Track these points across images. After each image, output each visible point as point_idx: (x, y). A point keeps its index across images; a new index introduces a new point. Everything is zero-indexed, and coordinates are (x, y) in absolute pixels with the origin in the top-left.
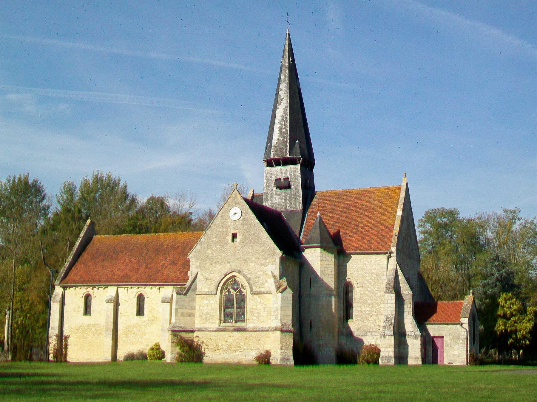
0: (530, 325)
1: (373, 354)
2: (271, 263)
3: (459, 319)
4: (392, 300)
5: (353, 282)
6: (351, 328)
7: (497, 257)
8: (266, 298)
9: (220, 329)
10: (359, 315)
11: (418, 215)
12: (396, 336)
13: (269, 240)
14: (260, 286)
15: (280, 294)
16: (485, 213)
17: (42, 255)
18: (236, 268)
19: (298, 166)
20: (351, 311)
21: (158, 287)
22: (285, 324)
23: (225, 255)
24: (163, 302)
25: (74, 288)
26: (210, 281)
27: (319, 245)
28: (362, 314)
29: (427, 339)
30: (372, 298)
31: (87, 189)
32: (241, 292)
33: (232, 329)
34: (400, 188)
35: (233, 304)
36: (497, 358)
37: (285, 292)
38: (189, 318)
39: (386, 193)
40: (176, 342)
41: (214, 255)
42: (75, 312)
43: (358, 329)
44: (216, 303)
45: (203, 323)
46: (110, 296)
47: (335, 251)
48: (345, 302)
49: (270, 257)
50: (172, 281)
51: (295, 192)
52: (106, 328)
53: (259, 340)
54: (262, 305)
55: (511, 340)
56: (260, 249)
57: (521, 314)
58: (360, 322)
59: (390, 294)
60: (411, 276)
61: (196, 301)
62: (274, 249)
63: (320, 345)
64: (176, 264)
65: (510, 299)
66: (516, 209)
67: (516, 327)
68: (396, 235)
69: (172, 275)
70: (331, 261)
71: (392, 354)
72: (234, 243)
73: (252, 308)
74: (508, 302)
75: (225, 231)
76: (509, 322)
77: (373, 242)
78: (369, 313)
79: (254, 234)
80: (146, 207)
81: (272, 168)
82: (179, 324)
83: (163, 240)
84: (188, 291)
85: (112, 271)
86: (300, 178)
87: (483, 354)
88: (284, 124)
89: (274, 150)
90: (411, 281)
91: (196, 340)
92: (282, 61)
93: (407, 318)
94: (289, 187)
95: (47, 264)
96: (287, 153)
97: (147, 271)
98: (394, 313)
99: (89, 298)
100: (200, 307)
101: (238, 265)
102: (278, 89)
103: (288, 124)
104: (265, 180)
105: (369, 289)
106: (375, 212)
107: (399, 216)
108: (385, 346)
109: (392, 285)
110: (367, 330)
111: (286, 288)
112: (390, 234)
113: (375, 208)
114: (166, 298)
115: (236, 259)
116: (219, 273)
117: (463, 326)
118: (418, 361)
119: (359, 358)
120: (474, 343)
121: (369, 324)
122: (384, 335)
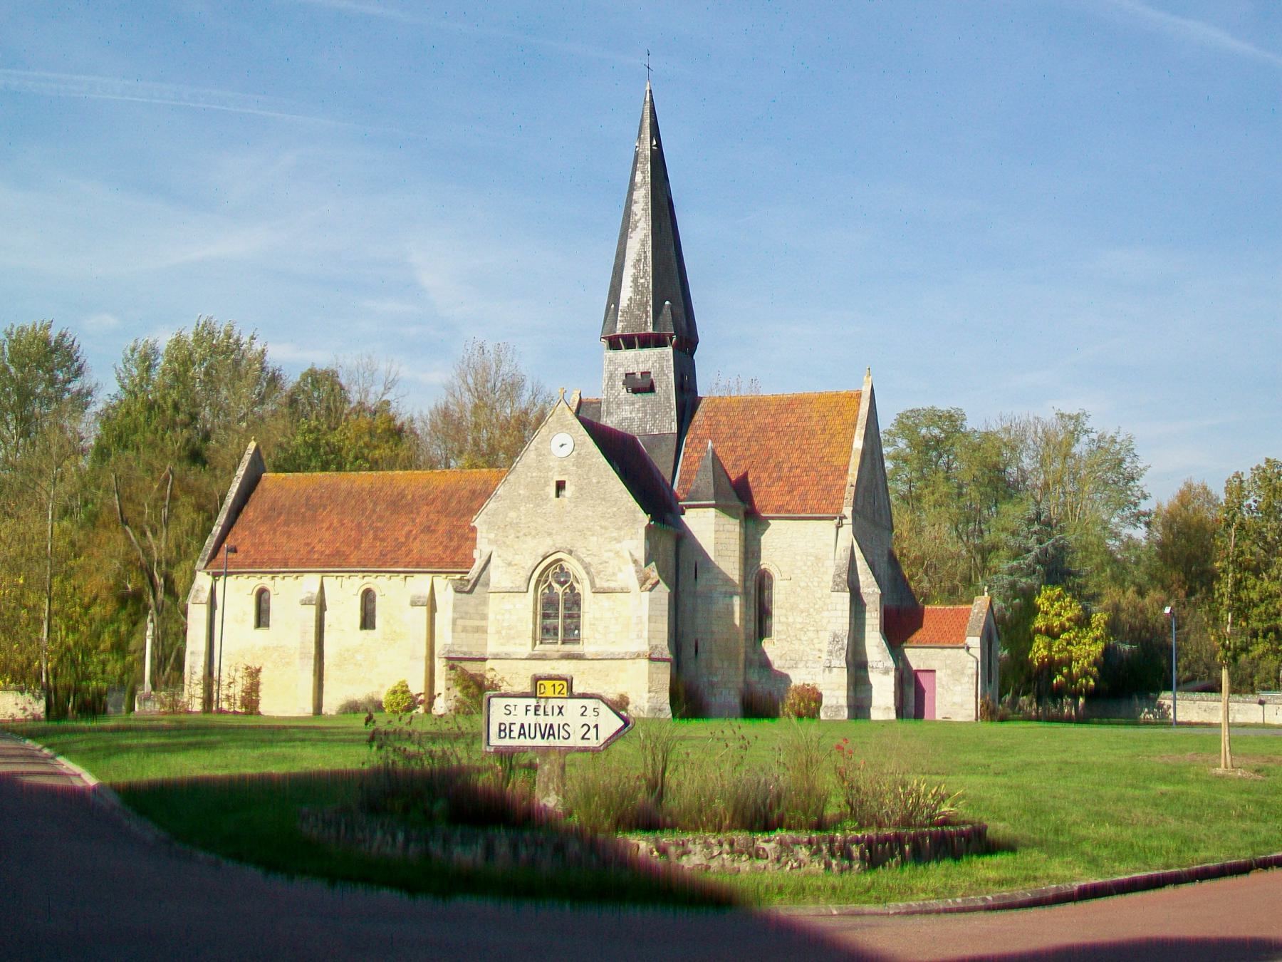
0: (1097, 649)
1: (808, 701)
3: (963, 637)
4: (844, 604)
5: (773, 570)
7: (1039, 515)
9: (535, 655)
11: (886, 422)
12: (852, 669)
15: (648, 592)
16: (1019, 418)
17: (117, 502)
19: (669, 351)
21: (402, 576)
22: (656, 647)
23: (544, 521)
24: (414, 604)
26: (515, 567)
27: (714, 502)
29: (906, 675)
31: (183, 359)
32: (572, 588)
33: (557, 655)
34: (859, 395)
35: (557, 609)
36: (1034, 713)
37: (656, 589)
38: (476, 635)
39: (832, 405)
40: (454, 680)
41: (523, 521)
43: (781, 657)
45: (502, 645)
46: (309, 592)
47: (741, 512)
48: (757, 605)
50: (430, 564)
52: (302, 653)
53: (607, 675)
55: (1059, 678)
57: (1080, 628)
60: (876, 558)
62: (634, 512)
63: (712, 684)
64: (433, 531)
65: (1059, 598)
66: (1080, 411)
67: (1070, 652)
68: (852, 486)
69: (428, 553)
71: (843, 702)
72: (561, 498)
73: (594, 618)
74: (1057, 605)
76: (1057, 642)
77: (809, 497)
79: (598, 482)
80: (299, 388)
81: (619, 352)
83: (403, 485)
84: (475, 585)
85: (308, 544)
86: (673, 374)
87: (1006, 705)
89: (622, 318)
90: (877, 568)
91: (489, 675)
92: (637, 144)
94: (651, 389)
95: (127, 521)
97: (378, 544)
98: (847, 627)
99: (265, 596)
101: (567, 539)
102: (630, 201)
103: (650, 269)
104: (605, 375)
105: (802, 584)
106: (813, 441)
107: (857, 449)
109: (845, 576)
111: (658, 582)
112: (840, 482)
113: (812, 433)
114: (419, 597)
119: (783, 708)
120: (990, 682)
121: (802, 648)
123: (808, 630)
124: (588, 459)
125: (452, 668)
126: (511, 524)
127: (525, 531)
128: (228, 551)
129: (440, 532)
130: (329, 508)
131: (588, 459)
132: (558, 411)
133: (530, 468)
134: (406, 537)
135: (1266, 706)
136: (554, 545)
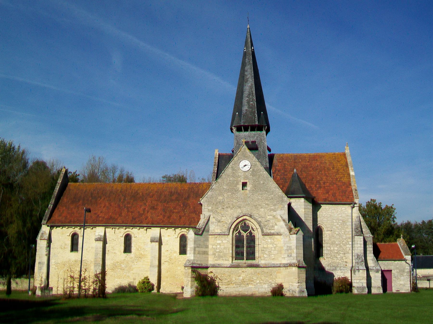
2: (280, 209)
4: (361, 241)
6: (322, 264)
8: (277, 239)
9: (234, 265)
10: (329, 253)
13: (278, 189)
14: (270, 228)
15: (295, 235)
18: (247, 213)
20: (321, 250)
21: (145, 228)
23: (236, 201)
24: (152, 241)
25: (61, 227)
28: (332, 252)
30: (339, 240)
32: (250, 233)
33: (245, 265)
37: (298, 233)
38: (204, 256)
41: (226, 201)
42: (62, 248)
43: (328, 265)
44: (228, 242)
46: (99, 235)
49: (278, 204)
51: (262, 153)
53: (271, 275)
54: (273, 245)
56: (269, 196)
58: (330, 259)
59: (359, 236)
61: (209, 240)
64: (156, 209)
70: (311, 209)
75: (236, 180)
78: (337, 251)
79: (263, 183)
82: (196, 261)
84: (203, 231)
88: (251, 98)
91: (210, 275)
93: (369, 255)
96: (256, 121)
99: (76, 237)
100: (213, 246)
105: (337, 233)
108: (360, 278)
110: (336, 265)
114: (155, 238)
115: (247, 205)
116: (230, 216)
117: (407, 261)
118: (379, 290)
121: (337, 261)
122: (358, 269)
123: (340, 253)
124: (258, 172)
125: (193, 271)
126: (220, 202)
127: (227, 205)
128: (86, 211)
129: (159, 209)
130: (103, 198)
131: (258, 172)
132: (242, 150)
133: (229, 176)
134: (143, 211)
135: (430, 281)
136: (242, 212)
